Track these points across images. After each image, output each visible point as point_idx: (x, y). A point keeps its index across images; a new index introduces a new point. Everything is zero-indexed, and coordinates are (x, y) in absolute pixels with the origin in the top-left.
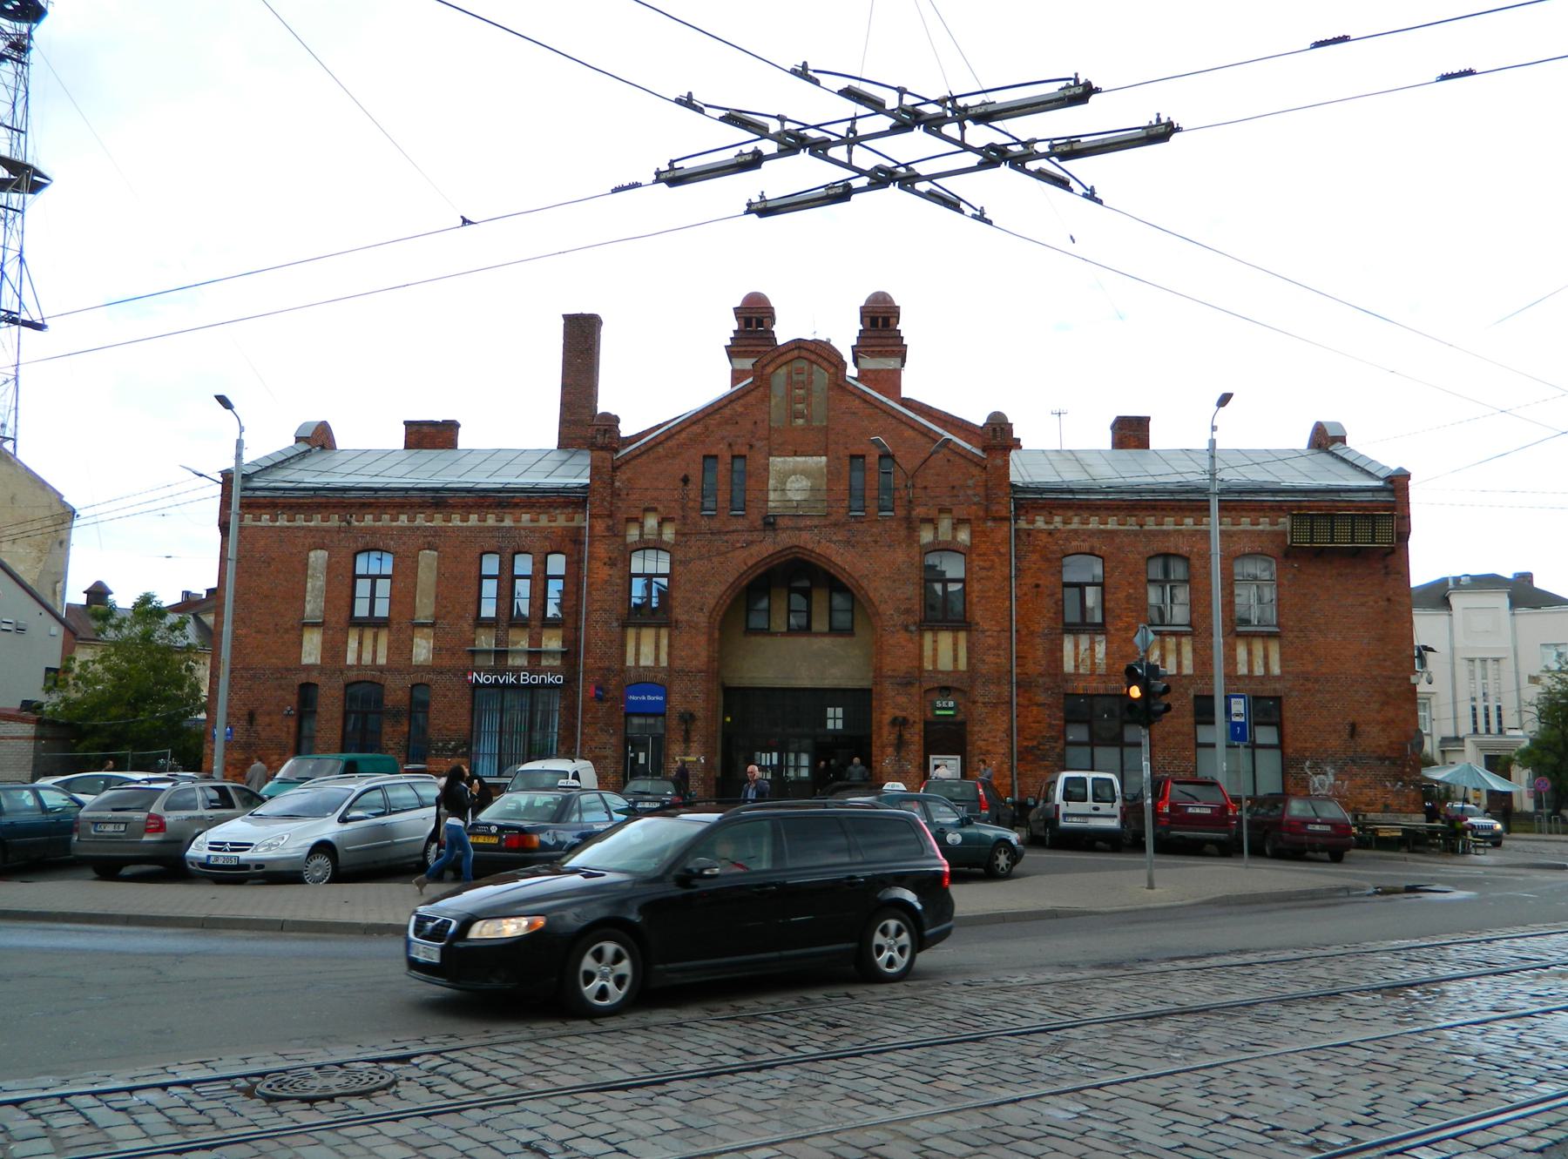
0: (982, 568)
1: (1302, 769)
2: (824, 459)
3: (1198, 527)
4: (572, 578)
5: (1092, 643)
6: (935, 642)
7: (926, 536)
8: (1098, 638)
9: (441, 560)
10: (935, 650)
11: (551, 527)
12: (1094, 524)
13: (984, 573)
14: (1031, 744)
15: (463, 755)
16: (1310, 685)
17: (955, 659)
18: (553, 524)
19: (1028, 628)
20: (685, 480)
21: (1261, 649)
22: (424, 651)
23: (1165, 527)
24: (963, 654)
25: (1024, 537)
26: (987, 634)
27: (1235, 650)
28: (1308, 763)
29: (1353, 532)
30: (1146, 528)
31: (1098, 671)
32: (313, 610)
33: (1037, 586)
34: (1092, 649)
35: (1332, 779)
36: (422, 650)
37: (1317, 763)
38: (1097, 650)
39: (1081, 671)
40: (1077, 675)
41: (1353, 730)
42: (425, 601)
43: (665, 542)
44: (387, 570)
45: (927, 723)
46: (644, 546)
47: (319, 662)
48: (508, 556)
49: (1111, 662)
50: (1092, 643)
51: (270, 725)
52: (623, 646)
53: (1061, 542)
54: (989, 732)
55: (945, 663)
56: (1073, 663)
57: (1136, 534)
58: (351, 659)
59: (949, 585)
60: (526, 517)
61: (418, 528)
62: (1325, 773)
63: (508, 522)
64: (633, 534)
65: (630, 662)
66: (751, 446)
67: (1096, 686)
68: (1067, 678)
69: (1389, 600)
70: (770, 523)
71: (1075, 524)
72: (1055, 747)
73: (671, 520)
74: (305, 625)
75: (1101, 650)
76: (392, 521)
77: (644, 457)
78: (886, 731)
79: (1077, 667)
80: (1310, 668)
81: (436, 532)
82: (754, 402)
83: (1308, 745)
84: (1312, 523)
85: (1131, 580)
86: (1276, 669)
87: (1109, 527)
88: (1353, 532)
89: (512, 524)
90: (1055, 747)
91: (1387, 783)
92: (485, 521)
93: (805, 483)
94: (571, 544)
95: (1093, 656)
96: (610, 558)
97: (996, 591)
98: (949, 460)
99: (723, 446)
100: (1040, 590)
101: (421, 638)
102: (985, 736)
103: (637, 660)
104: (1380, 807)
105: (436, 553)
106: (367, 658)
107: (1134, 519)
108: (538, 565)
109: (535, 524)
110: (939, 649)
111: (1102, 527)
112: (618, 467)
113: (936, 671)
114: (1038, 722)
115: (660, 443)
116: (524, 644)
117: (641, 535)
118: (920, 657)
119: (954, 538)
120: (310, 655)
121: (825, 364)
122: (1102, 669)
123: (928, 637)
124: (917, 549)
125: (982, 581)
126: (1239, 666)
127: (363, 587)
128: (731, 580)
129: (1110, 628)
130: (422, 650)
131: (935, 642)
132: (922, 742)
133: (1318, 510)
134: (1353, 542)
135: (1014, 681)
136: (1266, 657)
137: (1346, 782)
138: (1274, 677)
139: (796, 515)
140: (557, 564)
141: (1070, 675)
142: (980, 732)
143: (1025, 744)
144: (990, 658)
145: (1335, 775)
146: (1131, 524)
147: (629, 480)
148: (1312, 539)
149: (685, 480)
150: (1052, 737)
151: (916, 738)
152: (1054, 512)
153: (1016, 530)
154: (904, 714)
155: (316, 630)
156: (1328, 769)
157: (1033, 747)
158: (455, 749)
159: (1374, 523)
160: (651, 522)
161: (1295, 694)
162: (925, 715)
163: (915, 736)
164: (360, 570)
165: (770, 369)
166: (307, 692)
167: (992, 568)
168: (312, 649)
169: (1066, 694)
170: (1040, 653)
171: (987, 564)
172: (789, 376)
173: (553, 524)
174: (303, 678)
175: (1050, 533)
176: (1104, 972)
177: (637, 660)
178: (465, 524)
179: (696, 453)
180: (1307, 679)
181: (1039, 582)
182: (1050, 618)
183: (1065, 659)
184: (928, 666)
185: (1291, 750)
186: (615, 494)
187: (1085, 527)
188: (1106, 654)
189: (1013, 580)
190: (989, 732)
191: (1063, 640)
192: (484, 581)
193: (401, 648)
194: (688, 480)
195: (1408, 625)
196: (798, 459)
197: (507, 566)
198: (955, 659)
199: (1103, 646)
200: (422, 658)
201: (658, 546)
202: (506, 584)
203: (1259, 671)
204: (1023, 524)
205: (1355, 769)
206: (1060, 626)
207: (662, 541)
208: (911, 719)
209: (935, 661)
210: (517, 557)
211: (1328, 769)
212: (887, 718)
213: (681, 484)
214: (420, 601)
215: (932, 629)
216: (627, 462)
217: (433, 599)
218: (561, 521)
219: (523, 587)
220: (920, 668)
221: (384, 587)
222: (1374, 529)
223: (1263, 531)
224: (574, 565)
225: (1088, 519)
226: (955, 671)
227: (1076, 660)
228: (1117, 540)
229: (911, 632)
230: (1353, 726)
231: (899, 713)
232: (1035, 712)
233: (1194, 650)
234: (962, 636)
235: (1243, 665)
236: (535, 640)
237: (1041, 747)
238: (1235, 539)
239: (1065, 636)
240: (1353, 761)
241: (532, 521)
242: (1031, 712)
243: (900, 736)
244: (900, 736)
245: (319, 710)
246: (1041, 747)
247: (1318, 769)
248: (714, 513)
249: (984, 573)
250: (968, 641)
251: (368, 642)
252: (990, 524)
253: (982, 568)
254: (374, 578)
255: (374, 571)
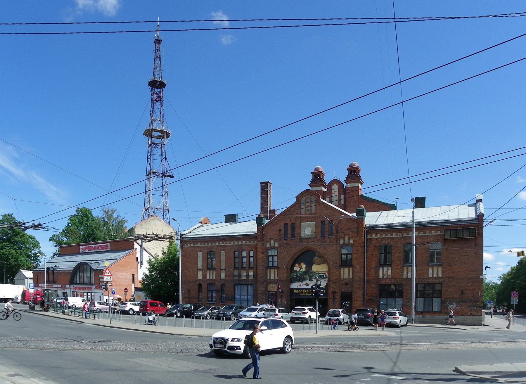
0: (356, 250)
1: (446, 304)
2: (315, 222)
3: (419, 235)
4: (255, 257)
5: (388, 269)
6: (344, 271)
7: (342, 242)
8: (389, 268)
9: (226, 253)
10: (344, 273)
11: (250, 244)
12: (389, 236)
13: (356, 252)
14: (370, 298)
15: (233, 301)
16: (450, 279)
17: (349, 276)
18: (250, 243)
19: (370, 266)
20: (280, 230)
21: (436, 270)
22: (223, 276)
23: (409, 235)
24: (351, 274)
25: (369, 241)
26: (357, 268)
27: (428, 270)
28: (448, 302)
29: (463, 234)
30: (404, 236)
31: (389, 277)
32: (200, 267)
33: (373, 254)
34: (388, 272)
35: (455, 306)
36: (223, 276)
37: (451, 302)
38: (389, 272)
39: (384, 278)
40: (383, 279)
41: (462, 292)
42: (223, 264)
43: (275, 247)
44: (276, 254)
45: (342, 293)
46: (271, 248)
47: (356, 214)
48: (248, 252)
49: (393, 275)
50: (388, 269)
51: (193, 293)
52: (267, 274)
53: (379, 242)
54: (357, 295)
55: (346, 276)
56: (382, 276)
57: (401, 238)
58: (208, 278)
59: (236, 267)
60: (244, 242)
61: (220, 246)
62: (453, 305)
63: (240, 243)
64: (268, 246)
65: (268, 278)
66: (296, 220)
67: (388, 282)
68: (380, 279)
69: (476, 253)
70: (301, 240)
71: (384, 236)
72: (376, 299)
73: (277, 241)
74: (198, 270)
75: (390, 272)
76: (215, 244)
77: (270, 225)
78: (330, 295)
79: (383, 277)
80: (450, 275)
81: (224, 246)
82: (296, 208)
83: (449, 297)
84: (450, 232)
85: (399, 251)
86: (440, 275)
87: (393, 236)
88: (463, 234)
89: (241, 244)
90: (376, 299)
91: (472, 307)
92: (239, 243)
93: (310, 229)
94: (255, 248)
95: (388, 274)
96: (263, 252)
97: (360, 257)
98: (347, 220)
99: (289, 221)
100: (373, 255)
101: (222, 273)
102: (356, 296)
103: (270, 278)
104: (469, 314)
105: (224, 252)
106: (211, 278)
107: (400, 233)
108: (247, 254)
109: (246, 244)
110: (345, 273)
111: (391, 236)
112: (264, 228)
113: (344, 279)
114: (372, 292)
115: (274, 221)
116: (245, 274)
117: (270, 246)
118: (340, 276)
119: (349, 242)
120: (200, 277)
121: (314, 196)
122: (390, 277)
123: (342, 270)
124: (338, 246)
125: (356, 254)
126: (429, 275)
127: (270, 259)
128: (291, 256)
129: (392, 265)
130: (223, 276)
131: (344, 271)
132: (340, 298)
133: (462, 227)
134: (463, 237)
135: (365, 281)
136: (437, 272)
137: (459, 307)
138: (439, 277)
139: (308, 239)
140: (252, 254)
141: (381, 279)
142: (355, 295)
143: (369, 298)
144: (358, 275)
145: (456, 305)
146: (400, 235)
147: (266, 231)
148: (450, 237)
149: (280, 230)
150: (376, 296)
151: (338, 297)
152: (378, 233)
153: (366, 239)
154: (335, 290)
155: (200, 271)
156: (454, 303)
157: (370, 299)
158: (231, 299)
159: (469, 231)
160: (272, 242)
161: (445, 282)
162: (341, 290)
163: (338, 297)
164: (269, 254)
165: (300, 199)
166: (200, 285)
167: (358, 250)
168: (200, 277)
169: (380, 284)
170: (373, 273)
171: (357, 249)
172: (305, 200)
173: (250, 243)
174: (198, 282)
175: (376, 239)
176: (396, 374)
177: (270, 278)
178: (230, 244)
179: (282, 224)
180: (449, 278)
181: (373, 253)
182: (376, 263)
183: (380, 274)
184: (342, 277)
185: (443, 299)
186: (263, 235)
187: (387, 237)
188: (391, 273)
189: (366, 253)
190: (357, 295)
191: (379, 269)
192: (243, 258)
193: (218, 275)
194: (281, 230)
195: (481, 261)
196: (308, 223)
197: (240, 254)
198: (349, 276)
199: (391, 270)
200: (223, 278)
201: (274, 248)
202: (240, 259)
203: (435, 276)
204: (369, 237)
205: (462, 304)
206: (379, 265)
207: (275, 247)
208: (337, 292)
209: (344, 276)
210: (243, 252)
211: (454, 303)
212: (331, 292)
213: (279, 232)
214: (222, 264)
215: (343, 267)
216: (266, 226)
217: (224, 263)
218: (252, 242)
219: (244, 260)
220: (340, 279)
221: (275, 258)
222: (469, 233)
223: (438, 235)
224: (256, 253)
225: (387, 234)
226: (349, 279)
227: (383, 275)
228: (395, 240)
229: (337, 269)
230: (462, 291)
231: (333, 290)
232: (371, 289)
233: (442, 271)
234: (351, 269)
235: (431, 274)
236: (247, 273)
237: (373, 299)
238: (430, 238)
239: (380, 268)
240: (462, 301)
241: (245, 243)
242: (370, 289)
243: (334, 296)
244: (334, 296)
245: (202, 290)
246: (373, 299)
247: (451, 304)
248: (404, 265)
249: (356, 252)
250: (352, 271)
251: (211, 274)
252: (358, 238)
253: (356, 250)
254: (273, 256)
255: (273, 254)
